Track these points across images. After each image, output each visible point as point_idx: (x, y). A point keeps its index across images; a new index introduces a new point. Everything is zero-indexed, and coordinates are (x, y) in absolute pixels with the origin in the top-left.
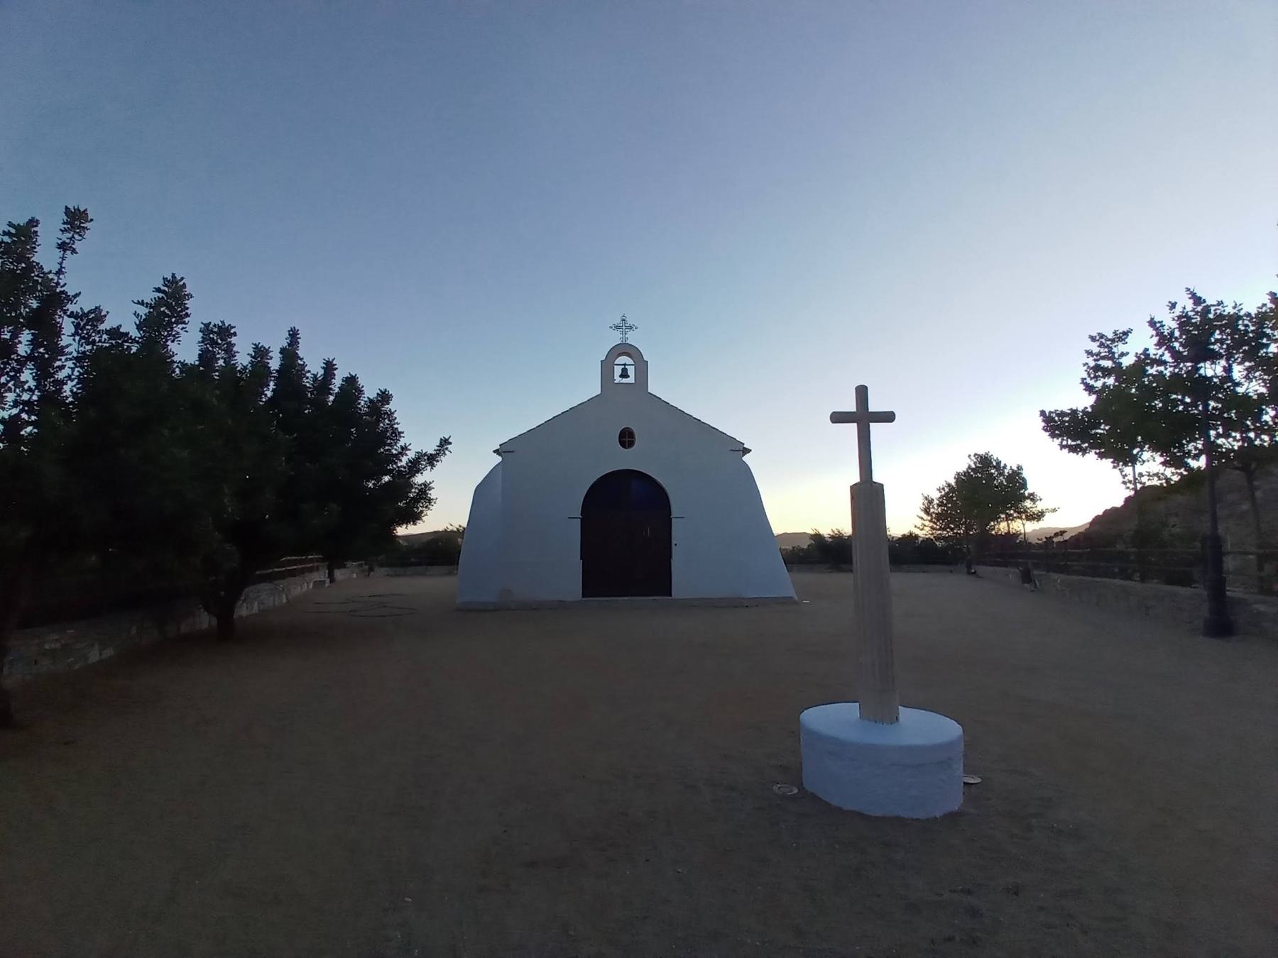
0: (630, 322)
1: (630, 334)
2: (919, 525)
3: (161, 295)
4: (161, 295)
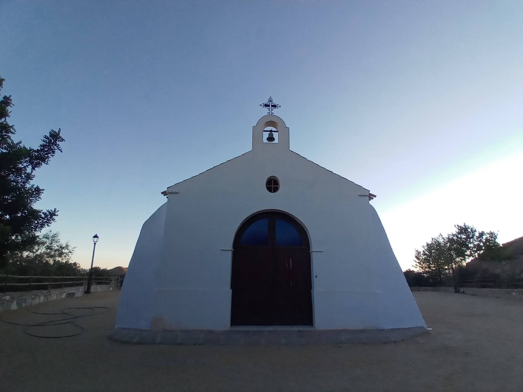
0: (275, 102)
1: (275, 111)
2: (414, 265)
3: (45, 143)
4: (45, 143)
